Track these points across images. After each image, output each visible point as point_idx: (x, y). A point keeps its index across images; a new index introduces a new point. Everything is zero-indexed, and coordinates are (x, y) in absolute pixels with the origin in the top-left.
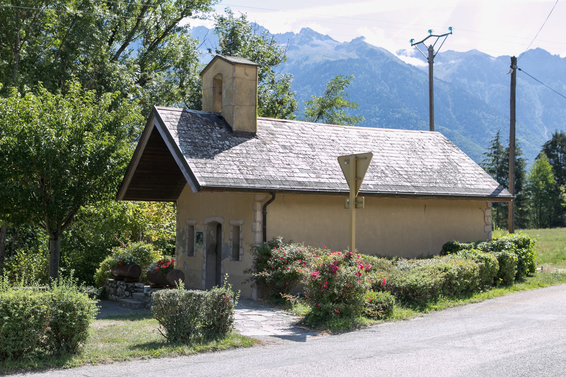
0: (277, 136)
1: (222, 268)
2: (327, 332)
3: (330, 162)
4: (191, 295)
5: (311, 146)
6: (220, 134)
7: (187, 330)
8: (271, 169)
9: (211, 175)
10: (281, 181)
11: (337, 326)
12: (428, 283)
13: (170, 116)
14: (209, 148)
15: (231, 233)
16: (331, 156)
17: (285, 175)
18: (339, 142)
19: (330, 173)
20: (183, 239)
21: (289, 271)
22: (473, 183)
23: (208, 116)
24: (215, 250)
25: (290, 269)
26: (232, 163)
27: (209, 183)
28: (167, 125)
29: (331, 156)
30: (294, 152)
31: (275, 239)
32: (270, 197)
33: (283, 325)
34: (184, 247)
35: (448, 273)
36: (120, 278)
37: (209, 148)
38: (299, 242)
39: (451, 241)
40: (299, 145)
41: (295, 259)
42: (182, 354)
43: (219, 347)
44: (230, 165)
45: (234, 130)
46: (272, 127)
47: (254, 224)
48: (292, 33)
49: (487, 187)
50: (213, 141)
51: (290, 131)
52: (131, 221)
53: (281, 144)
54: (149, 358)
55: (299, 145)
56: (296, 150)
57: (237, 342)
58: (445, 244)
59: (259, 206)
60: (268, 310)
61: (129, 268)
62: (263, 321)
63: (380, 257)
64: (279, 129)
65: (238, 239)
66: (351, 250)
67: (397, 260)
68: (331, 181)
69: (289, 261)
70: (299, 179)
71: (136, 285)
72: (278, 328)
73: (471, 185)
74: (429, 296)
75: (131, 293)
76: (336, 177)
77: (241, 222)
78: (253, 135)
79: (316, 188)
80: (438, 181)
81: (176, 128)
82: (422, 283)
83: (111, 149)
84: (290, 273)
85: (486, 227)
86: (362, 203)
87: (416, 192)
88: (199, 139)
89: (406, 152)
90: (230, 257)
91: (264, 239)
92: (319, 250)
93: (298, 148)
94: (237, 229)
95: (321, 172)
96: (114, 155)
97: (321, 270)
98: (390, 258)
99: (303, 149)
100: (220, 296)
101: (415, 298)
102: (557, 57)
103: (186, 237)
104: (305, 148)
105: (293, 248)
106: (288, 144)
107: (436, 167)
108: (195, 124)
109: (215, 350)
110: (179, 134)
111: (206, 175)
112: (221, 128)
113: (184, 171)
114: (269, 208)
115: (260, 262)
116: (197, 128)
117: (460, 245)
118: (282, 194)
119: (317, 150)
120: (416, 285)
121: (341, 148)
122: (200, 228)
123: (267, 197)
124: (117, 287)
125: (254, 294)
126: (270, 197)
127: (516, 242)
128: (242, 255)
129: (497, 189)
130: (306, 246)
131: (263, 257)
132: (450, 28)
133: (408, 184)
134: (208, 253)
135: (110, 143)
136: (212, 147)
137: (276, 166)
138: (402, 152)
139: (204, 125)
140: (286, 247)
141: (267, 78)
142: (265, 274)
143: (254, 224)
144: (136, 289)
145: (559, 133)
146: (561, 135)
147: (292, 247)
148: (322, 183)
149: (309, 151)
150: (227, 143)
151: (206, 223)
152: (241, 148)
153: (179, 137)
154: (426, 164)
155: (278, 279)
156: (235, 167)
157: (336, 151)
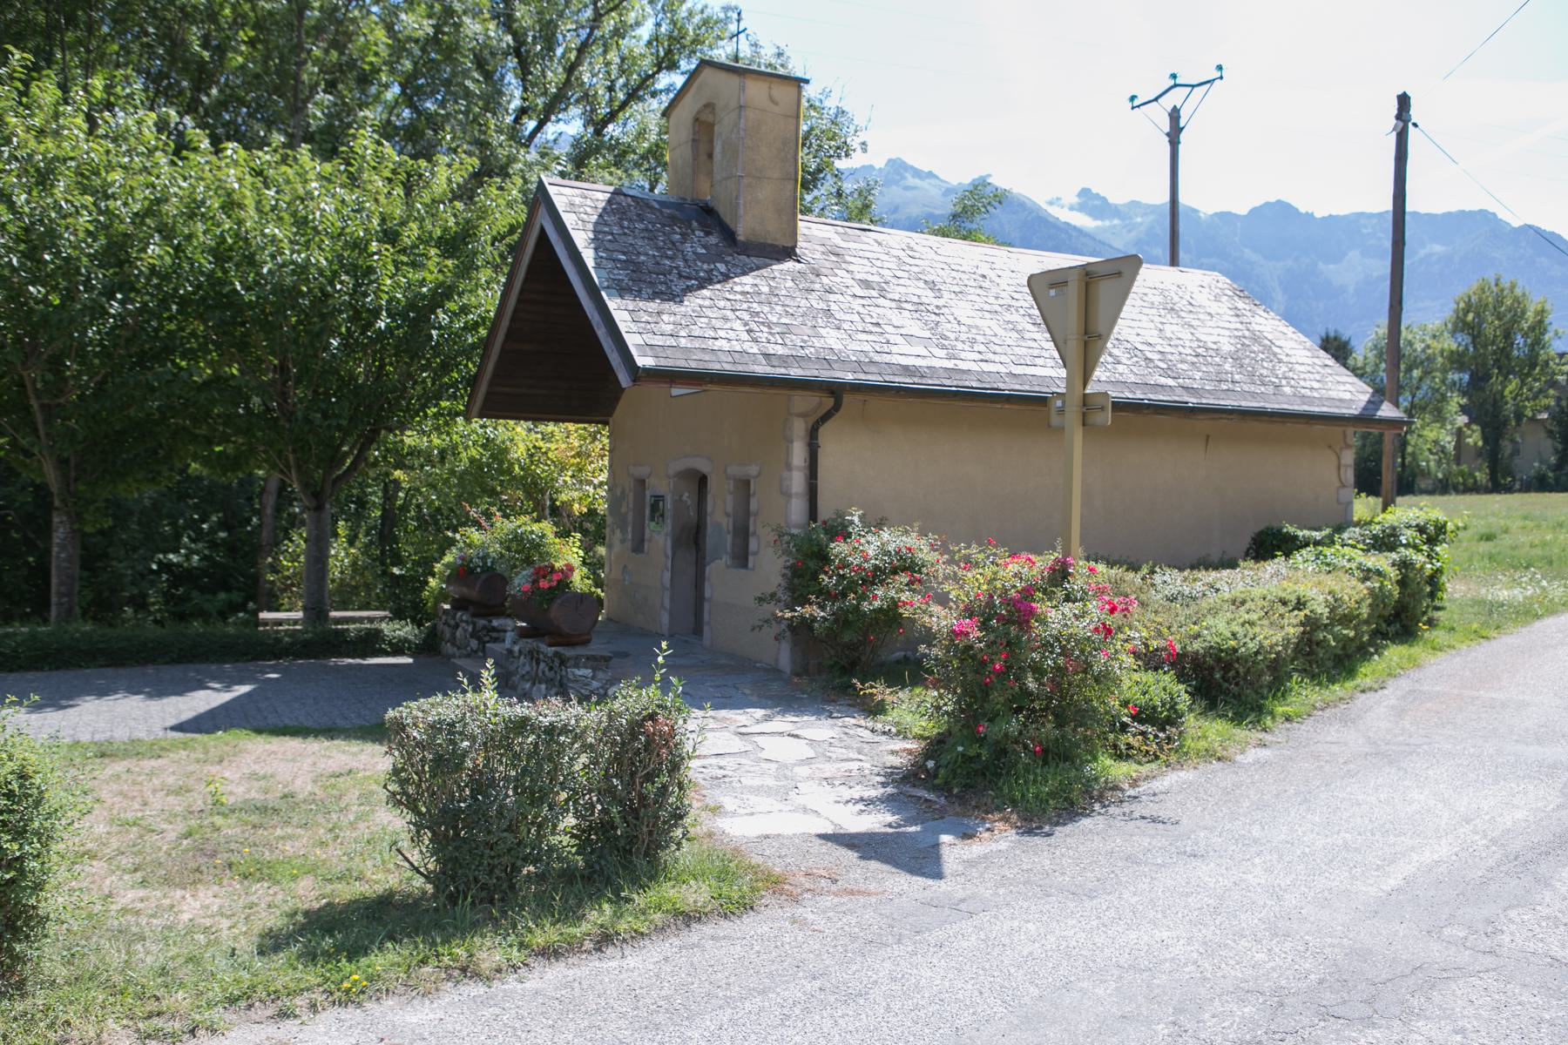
0: (848, 258)
1: (707, 584)
2: (1006, 820)
3: (978, 322)
4: (521, 725)
5: (932, 285)
6: (704, 247)
7: (505, 860)
8: (834, 333)
9: (671, 341)
10: (859, 362)
11: (1036, 797)
12: (1266, 643)
13: (579, 206)
14: (674, 277)
15: (729, 498)
16: (981, 310)
17: (867, 348)
18: (997, 280)
19: (982, 348)
20: (623, 510)
21: (877, 604)
22: (1316, 385)
23: (679, 206)
24: (692, 538)
25: (879, 597)
26: (729, 313)
27: (663, 362)
28: (569, 220)
29: (981, 310)
30: (890, 296)
31: (841, 515)
32: (829, 402)
33: (862, 779)
34: (624, 531)
35: (1307, 612)
36: (459, 604)
37: (674, 277)
38: (903, 522)
39: (1276, 525)
40: (901, 281)
41: (895, 571)
42: (468, 971)
43: (622, 926)
44: (726, 319)
45: (741, 238)
46: (837, 240)
47: (785, 474)
48: (872, 167)
49: (1347, 396)
50: (686, 261)
51: (879, 249)
52: (522, 469)
53: (858, 276)
54: (313, 1007)
55: (901, 281)
56: (896, 292)
57: (695, 894)
58: (1261, 533)
59: (799, 428)
60: (818, 713)
61: (479, 582)
62: (802, 762)
63: (1111, 564)
64: (851, 245)
65: (747, 513)
66: (1067, 553)
67: (1153, 572)
68: (986, 367)
69: (877, 576)
70: (904, 361)
71: (495, 623)
72: (847, 794)
73: (1312, 389)
74: (1268, 678)
75: (482, 643)
76: (997, 358)
77: (753, 470)
78: (788, 253)
79: (947, 382)
80: (1237, 377)
81: (591, 227)
82: (1251, 645)
83: (443, 294)
84: (880, 610)
85: (1342, 492)
86: (1103, 409)
87: (1192, 401)
88: (647, 254)
89: (1154, 311)
90: (725, 559)
91: (813, 513)
92: (974, 549)
93: (902, 290)
94: (744, 485)
95: (960, 346)
96: (451, 306)
97: (982, 612)
98: (1135, 568)
99: (911, 290)
100: (635, 727)
101: (1231, 685)
102: (1310, 216)
103: (627, 507)
104: (917, 290)
105: (891, 539)
106: (876, 278)
107: (1226, 348)
108: (642, 221)
109: (605, 939)
110: (598, 242)
111: (658, 340)
112: (708, 234)
113: (601, 333)
114: (827, 434)
115: (799, 576)
116: (646, 230)
117: (1300, 533)
118: (859, 397)
119: (946, 295)
120: (1235, 650)
121: (1003, 294)
122: (660, 485)
123: (820, 404)
124: (457, 626)
125: (784, 658)
126: (829, 402)
127: (1421, 529)
128: (756, 553)
129: (1369, 402)
130: (923, 533)
131: (809, 563)
132: (1220, 68)
133: (1171, 382)
134: (675, 547)
135: (441, 277)
136: (680, 276)
137: (845, 326)
138: (1145, 311)
139: (664, 225)
140: (869, 538)
141: (827, 185)
142: (812, 611)
143: (785, 474)
144: (494, 635)
145: (1332, 334)
146: (1336, 338)
147: (885, 535)
148: (963, 371)
149: (928, 296)
150: (722, 267)
151: (671, 472)
152: (758, 281)
153: (596, 249)
154: (1203, 338)
155: (847, 624)
156: (738, 325)
157: (991, 300)
